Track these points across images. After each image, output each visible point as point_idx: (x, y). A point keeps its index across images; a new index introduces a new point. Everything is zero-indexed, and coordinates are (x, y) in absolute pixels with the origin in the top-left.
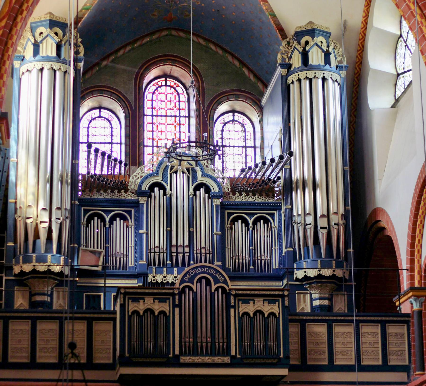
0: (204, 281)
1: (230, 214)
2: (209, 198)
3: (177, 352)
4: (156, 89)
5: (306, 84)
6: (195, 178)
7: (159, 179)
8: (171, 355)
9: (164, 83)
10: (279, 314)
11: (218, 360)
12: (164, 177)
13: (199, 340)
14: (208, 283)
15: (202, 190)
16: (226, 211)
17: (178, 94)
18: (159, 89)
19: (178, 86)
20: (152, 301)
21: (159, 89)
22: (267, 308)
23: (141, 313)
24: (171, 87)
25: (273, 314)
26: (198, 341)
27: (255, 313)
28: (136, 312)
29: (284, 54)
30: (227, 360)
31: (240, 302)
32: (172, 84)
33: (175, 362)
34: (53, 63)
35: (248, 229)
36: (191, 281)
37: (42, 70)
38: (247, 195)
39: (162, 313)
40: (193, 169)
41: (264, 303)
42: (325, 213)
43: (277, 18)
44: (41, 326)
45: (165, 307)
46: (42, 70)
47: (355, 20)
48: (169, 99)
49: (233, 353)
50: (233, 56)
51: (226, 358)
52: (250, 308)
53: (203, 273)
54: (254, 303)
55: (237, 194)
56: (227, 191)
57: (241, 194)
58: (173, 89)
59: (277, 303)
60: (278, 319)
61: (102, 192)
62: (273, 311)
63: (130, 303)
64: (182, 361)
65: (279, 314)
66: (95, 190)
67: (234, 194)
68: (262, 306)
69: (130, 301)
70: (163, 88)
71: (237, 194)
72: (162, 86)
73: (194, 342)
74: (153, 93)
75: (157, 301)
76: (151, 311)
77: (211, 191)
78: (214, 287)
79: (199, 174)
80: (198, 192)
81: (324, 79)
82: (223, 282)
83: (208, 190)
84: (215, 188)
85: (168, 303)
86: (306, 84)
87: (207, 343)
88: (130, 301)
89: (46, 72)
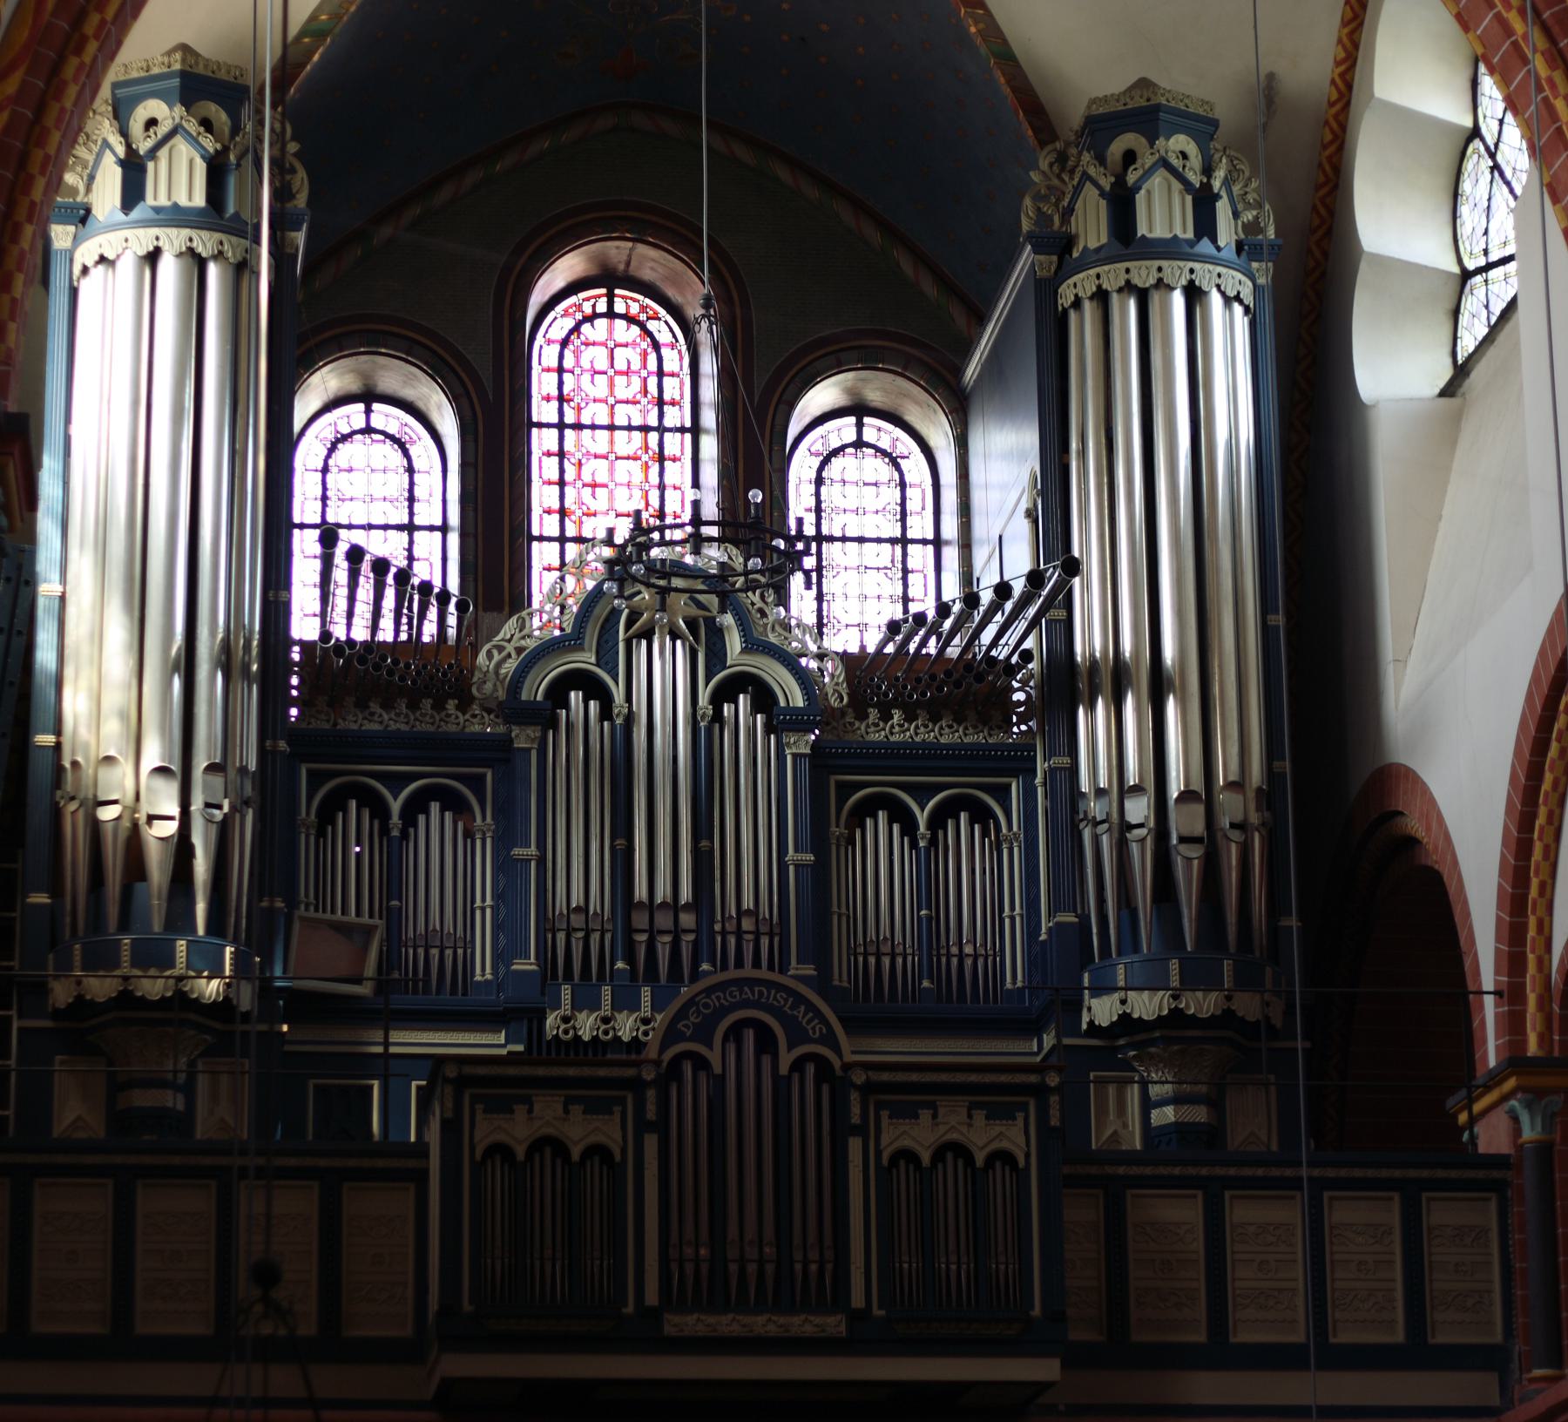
1: (846, 790)
2: (769, 729)
3: (652, 1298)
4: (576, 329)
6: (716, 656)
7: (585, 659)
9: (602, 307)
11: (801, 1325)
12: (606, 657)
14: (766, 1042)
16: (833, 779)
17: (656, 346)
18: (586, 328)
21: (586, 328)
24: (630, 319)
25: (1005, 1157)
28: (500, 1151)
29: (1045, 198)
30: (835, 1324)
32: (634, 309)
35: (914, 845)
36: (704, 1034)
38: (910, 717)
39: (597, 1151)
40: (710, 622)
41: (970, 1116)
45: (609, 1131)
46: (153, 258)
48: (620, 365)
49: (857, 1301)
51: (831, 1320)
52: (921, 1136)
53: (746, 1004)
54: (935, 1116)
55: (873, 714)
57: (886, 717)
59: (1020, 1116)
60: (1021, 1175)
63: (479, 1117)
64: (668, 1330)
67: (863, 716)
68: (964, 1129)
70: (601, 323)
71: (873, 714)
72: (594, 316)
74: (565, 343)
77: (776, 701)
78: (786, 1059)
80: (727, 709)
81: (1194, 295)
82: (822, 1041)
83: (764, 698)
88: (479, 1107)
89: (169, 267)
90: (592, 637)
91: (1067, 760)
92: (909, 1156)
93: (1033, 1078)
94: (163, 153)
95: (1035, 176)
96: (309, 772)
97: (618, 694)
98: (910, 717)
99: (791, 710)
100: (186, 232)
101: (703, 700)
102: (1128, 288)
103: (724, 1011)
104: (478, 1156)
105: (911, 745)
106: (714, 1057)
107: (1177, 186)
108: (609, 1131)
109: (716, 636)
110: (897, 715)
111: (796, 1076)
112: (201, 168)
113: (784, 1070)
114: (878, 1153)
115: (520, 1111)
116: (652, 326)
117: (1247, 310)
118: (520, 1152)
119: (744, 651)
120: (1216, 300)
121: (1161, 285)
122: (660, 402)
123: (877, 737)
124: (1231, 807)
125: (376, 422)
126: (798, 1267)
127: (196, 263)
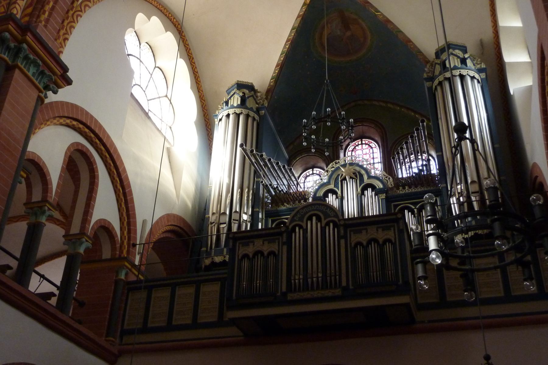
0: (314, 218)
1: (396, 206)
2: (376, 195)
3: (284, 289)
4: (355, 148)
5: (447, 85)
6: (362, 180)
7: (332, 186)
8: (279, 294)
9: (360, 143)
10: (395, 239)
11: (328, 293)
12: (336, 185)
13: (309, 276)
14: (319, 219)
15: (370, 190)
16: (392, 204)
17: (372, 148)
18: (357, 147)
19: (372, 143)
20: (262, 243)
21: (357, 147)
22: (381, 236)
23: (251, 256)
24: (366, 144)
25: (389, 241)
26: (308, 277)
27: (369, 242)
28: (246, 256)
29: (429, 73)
30: (338, 292)
31: (352, 233)
32: (367, 142)
33: (284, 301)
34: (236, 109)
35: (414, 217)
36: (301, 219)
37: (228, 116)
38: (410, 187)
39: (272, 253)
40: (359, 173)
41: (377, 230)
42: (476, 179)
43: (423, 54)
44: (180, 291)
45: (274, 247)
46: (228, 116)
47: (488, 35)
48: (364, 153)
49: (344, 284)
50: (408, 109)
51: (337, 291)
52: (363, 238)
53: (313, 210)
54: (367, 232)
55: (401, 188)
56: (390, 186)
57: (404, 188)
58: (367, 146)
59: (392, 229)
60: (394, 244)
61: (285, 204)
62: (388, 237)
63: (240, 247)
64: (289, 298)
65: (395, 239)
66: (280, 204)
67: (398, 189)
68: (376, 234)
69: (241, 245)
70: (360, 146)
71: (401, 188)
72: (358, 145)
73: (303, 279)
74: (352, 151)
75: (266, 243)
76: (261, 253)
77: (376, 187)
78: (324, 222)
79: (365, 177)
80: (366, 192)
81: (462, 77)
82: (334, 217)
83: (373, 187)
84: (379, 185)
85: (277, 244)
86: (447, 85)
87: (318, 277)
88: (241, 245)
89: (231, 117)
90: (332, 182)
91: (445, 185)
92: (360, 244)
93: (394, 217)
94: (232, 98)
95: (426, 69)
96: (272, 220)
97: (339, 192)
98: (410, 187)
99: (380, 189)
100: (234, 109)
101: (359, 190)
102: (446, 79)
103: (307, 213)
104: (240, 258)
105: (411, 193)
106: (304, 225)
107: (455, 58)
108: (274, 247)
109: (361, 176)
110: (407, 187)
111: (327, 228)
112: (239, 99)
113: (323, 225)
114: (351, 244)
115: (251, 246)
116: (371, 144)
117: (478, 82)
118: (251, 256)
119: (368, 179)
120: (469, 79)
121: (453, 76)
122: (373, 158)
123: (401, 192)
124: (486, 183)
125: (315, 172)
126: (328, 278)
127: (238, 115)
